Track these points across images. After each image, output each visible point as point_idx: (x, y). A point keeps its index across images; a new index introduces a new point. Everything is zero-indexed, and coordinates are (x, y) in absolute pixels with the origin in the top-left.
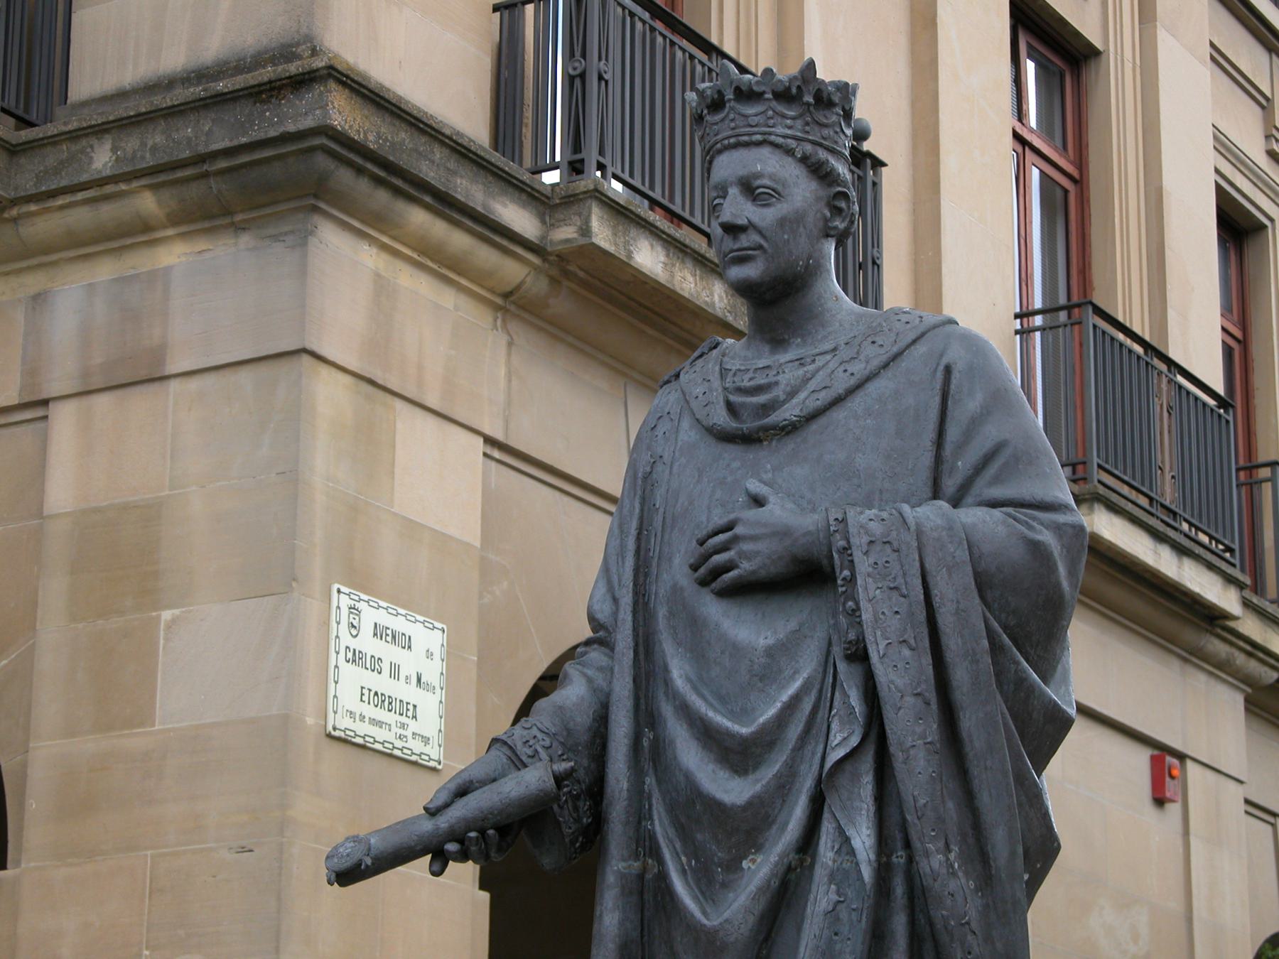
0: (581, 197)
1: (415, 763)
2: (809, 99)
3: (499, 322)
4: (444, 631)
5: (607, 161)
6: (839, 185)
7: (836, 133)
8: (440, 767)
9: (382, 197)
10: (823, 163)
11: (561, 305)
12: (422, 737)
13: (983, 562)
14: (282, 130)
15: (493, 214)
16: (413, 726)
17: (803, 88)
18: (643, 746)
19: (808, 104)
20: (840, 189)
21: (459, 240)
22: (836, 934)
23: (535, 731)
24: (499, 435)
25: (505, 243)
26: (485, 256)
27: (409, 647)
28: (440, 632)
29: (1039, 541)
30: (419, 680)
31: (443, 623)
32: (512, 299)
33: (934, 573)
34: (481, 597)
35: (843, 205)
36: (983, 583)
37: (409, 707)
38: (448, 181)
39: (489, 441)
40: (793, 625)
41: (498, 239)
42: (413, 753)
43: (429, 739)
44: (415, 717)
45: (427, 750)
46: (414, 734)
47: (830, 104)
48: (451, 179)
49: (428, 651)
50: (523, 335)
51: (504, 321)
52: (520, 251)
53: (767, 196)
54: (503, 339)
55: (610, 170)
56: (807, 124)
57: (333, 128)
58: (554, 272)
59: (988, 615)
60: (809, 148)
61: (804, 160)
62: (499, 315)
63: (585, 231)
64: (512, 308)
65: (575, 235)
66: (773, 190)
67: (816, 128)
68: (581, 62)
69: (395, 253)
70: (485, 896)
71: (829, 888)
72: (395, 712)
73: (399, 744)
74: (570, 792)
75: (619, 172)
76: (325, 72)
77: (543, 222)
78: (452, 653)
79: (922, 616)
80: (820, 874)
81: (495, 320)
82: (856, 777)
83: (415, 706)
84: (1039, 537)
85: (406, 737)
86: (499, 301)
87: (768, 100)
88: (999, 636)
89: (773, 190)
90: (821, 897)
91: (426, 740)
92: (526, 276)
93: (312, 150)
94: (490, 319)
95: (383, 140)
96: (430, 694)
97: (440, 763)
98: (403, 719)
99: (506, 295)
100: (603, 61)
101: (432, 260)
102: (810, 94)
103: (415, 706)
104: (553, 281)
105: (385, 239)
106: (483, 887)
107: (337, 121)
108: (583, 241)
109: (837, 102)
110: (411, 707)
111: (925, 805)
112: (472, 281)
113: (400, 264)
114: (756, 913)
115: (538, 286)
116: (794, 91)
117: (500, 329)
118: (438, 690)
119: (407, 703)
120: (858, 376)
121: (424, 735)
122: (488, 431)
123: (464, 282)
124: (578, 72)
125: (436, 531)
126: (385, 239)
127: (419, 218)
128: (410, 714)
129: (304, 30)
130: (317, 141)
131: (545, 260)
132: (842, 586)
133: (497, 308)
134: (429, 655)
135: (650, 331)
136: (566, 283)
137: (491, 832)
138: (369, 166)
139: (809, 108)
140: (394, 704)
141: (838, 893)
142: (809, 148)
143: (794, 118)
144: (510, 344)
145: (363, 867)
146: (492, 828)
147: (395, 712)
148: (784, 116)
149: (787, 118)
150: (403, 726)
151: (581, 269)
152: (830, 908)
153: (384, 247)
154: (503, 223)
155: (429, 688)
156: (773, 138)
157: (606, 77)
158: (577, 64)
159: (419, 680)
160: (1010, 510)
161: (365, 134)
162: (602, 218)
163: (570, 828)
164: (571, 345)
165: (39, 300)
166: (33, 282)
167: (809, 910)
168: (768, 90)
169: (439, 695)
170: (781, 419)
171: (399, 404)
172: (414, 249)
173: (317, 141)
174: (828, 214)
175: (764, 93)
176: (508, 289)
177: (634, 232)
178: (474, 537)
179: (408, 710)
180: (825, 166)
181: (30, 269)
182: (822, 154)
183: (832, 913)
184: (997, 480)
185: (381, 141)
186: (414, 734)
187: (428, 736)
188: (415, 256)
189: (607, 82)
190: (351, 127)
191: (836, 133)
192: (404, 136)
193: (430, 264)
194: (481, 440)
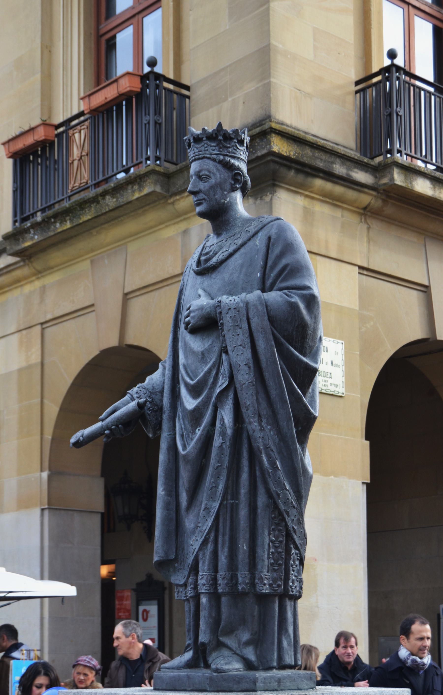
0: (389, 165)
1: (332, 395)
2: (220, 138)
3: (363, 220)
4: (343, 344)
5: (402, 149)
6: (236, 170)
7: (235, 149)
8: (343, 395)
9: (300, 178)
10: (228, 162)
11: (389, 210)
12: (335, 385)
13: (272, 312)
14: (256, 155)
15: (353, 178)
16: (330, 381)
17: (218, 134)
18: (177, 391)
19: (220, 140)
20: (236, 172)
21: (338, 189)
22: (222, 454)
23: (141, 389)
24: (365, 265)
25: (359, 188)
26: (351, 194)
27: (327, 351)
28: (341, 344)
29: (293, 302)
30: (332, 363)
31: (342, 340)
32: (368, 210)
33: (252, 318)
34: (360, 329)
35: (239, 178)
36: (271, 319)
37: (328, 374)
38: (329, 166)
39: (360, 267)
40: (210, 343)
41: (356, 187)
42: (331, 391)
43: (338, 385)
44: (331, 377)
45: (337, 389)
46: (330, 384)
47: (231, 139)
48: (331, 165)
49: (336, 352)
50: (376, 225)
51: (365, 219)
52: (366, 190)
53: (205, 179)
54: (365, 226)
55: (404, 152)
56: (221, 148)
57: (274, 152)
58: (384, 197)
59: (275, 332)
60: (222, 157)
61: (220, 162)
62: (363, 217)
63: (392, 179)
64: (369, 214)
65: (388, 181)
66: (208, 176)
67: (225, 149)
68: (389, 110)
69: (312, 198)
70: (368, 443)
71: (219, 438)
72: (322, 376)
73: (324, 388)
74: (153, 409)
75: (409, 152)
76: (269, 130)
77: (376, 177)
78: (348, 352)
79: (247, 335)
80: (217, 433)
81: (361, 219)
82: (227, 397)
83: (331, 373)
84: (293, 300)
85: (327, 385)
86: (362, 211)
87: (204, 140)
88: (281, 340)
89: (208, 176)
90: (217, 441)
91: (336, 386)
92: (371, 200)
93: (268, 162)
94: (359, 219)
95: (298, 154)
96: (337, 368)
97: (343, 394)
98: (326, 379)
99: (365, 208)
100: (399, 107)
101: (329, 198)
102: (221, 136)
103: (331, 373)
104: (384, 200)
105: (307, 193)
106: (367, 439)
107: (275, 149)
108: (391, 183)
109: (233, 137)
110: (329, 374)
111: (249, 405)
112: (349, 205)
113: (315, 202)
114: (197, 448)
115: (377, 203)
116: (214, 135)
117: (363, 222)
118: (341, 366)
119: (327, 373)
120: (238, 244)
121: (336, 384)
122: (360, 264)
123: (345, 206)
124: (388, 113)
125: (338, 305)
126: (307, 193)
127: (319, 183)
128: (329, 376)
129: (268, 113)
130: (269, 158)
131: (378, 192)
132: (220, 326)
133: (361, 214)
134: (336, 353)
135: (432, 216)
136: (389, 201)
137: (120, 426)
138: (293, 165)
139: (221, 142)
140: (321, 373)
141: (223, 439)
142: (222, 157)
143: (215, 147)
144: (369, 228)
145: (80, 441)
146: (120, 424)
147: (322, 376)
148: (211, 146)
149: (212, 147)
150: (326, 381)
151: (395, 194)
152: (220, 445)
153: (307, 196)
154: (356, 180)
155: (336, 366)
156: (206, 155)
157: (400, 114)
158: (387, 110)
159: (332, 363)
160: (286, 291)
161: (289, 152)
162: (399, 172)
163: (153, 422)
164: (397, 225)
165: (186, 232)
166: (183, 226)
167: (213, 446)
168: (204, 137)
169: (342, 368)
170: (210, 264)
171: (318, 258)
172: (320, 195)
173: (269, 158)
174: (233, 182)
175: (203, 138)
176: (364, 206)
177: (414, 176)
178: (355, 305)
179: (327, 375)
180: (229, 164)
181: (181, 221)
182: (228, 159)
183: (221, 447)
184: (284, 280)
185: (297, 154)
186: (330, 384)
187: (337, 384)
188: (321, 198)
189: (401, 116)
190: (282, 151)
191: (235, 149)
192: (308, 151)
193: (328, 200)
194: (357, 268)
